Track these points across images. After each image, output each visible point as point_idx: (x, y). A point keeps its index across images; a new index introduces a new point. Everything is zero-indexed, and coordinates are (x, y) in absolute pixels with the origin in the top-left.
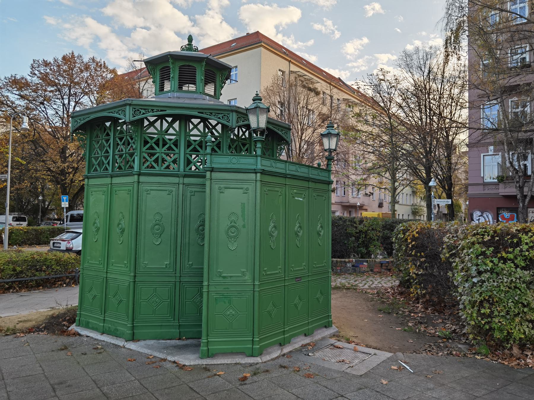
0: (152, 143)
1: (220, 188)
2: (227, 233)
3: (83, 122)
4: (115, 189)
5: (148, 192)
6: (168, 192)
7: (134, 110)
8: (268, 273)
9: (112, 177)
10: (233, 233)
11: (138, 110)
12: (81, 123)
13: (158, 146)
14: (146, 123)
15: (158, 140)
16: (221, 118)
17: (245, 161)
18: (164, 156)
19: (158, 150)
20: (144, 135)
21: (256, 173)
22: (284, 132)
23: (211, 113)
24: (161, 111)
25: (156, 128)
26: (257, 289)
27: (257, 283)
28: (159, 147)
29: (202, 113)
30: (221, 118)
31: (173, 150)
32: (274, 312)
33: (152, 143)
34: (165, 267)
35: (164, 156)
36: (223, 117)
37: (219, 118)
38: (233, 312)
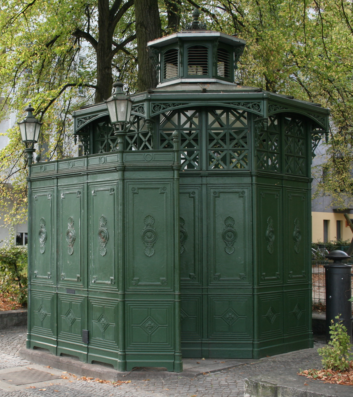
0: (217, 139)
1: (133, 189)
2: (143, 237)
3: (88, 121)
4: (59, 189)
5: (136, 191)
6: (160, 191)
7: (153, 105)
8: (294, 276)
9: (57, 179)
10: (150, 238)
11: (158, 106)
12: (86, 123)
13: (225, 143)
14: (162, 119)
15: (225, 135)
16: (251, 107)
17: (164, 158)
18: (232, 153)
19: (225, 147)
20: (209, 131)
21: (173, 170)
22: (320, 118)
23: (239, 103)
24: (183, 104)
25: (213, 123)
26: (255, 293)
27: (256, 287)
28: (226, 144)
29: (229, 103)
30: (251, 107)
31: (221, 146)
32: (273, 318)
33: (217, 139)
34: (76, 280)
35: (232, 153)
36: (253, 107)
37: (249, 108)
38: (233, 316)
